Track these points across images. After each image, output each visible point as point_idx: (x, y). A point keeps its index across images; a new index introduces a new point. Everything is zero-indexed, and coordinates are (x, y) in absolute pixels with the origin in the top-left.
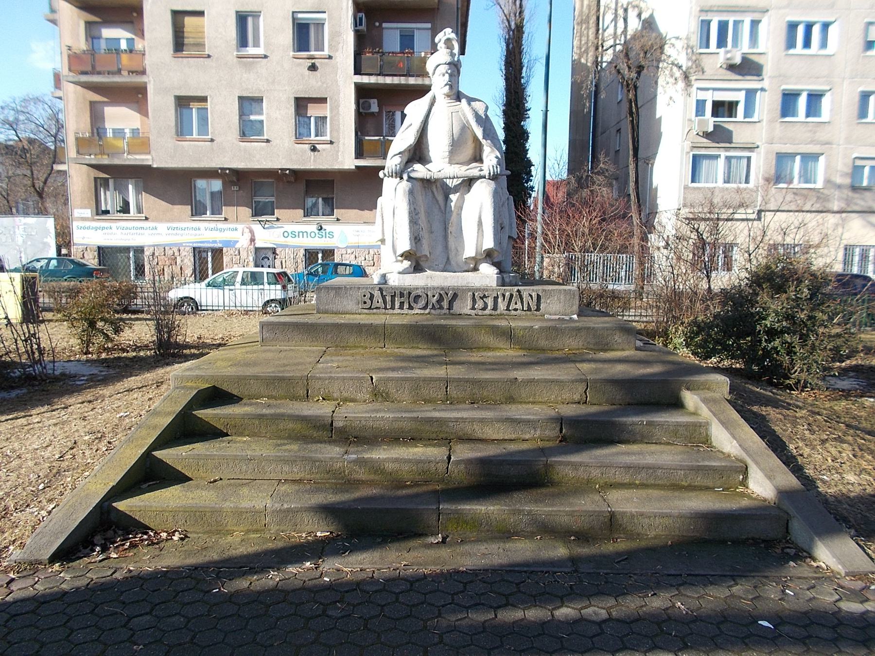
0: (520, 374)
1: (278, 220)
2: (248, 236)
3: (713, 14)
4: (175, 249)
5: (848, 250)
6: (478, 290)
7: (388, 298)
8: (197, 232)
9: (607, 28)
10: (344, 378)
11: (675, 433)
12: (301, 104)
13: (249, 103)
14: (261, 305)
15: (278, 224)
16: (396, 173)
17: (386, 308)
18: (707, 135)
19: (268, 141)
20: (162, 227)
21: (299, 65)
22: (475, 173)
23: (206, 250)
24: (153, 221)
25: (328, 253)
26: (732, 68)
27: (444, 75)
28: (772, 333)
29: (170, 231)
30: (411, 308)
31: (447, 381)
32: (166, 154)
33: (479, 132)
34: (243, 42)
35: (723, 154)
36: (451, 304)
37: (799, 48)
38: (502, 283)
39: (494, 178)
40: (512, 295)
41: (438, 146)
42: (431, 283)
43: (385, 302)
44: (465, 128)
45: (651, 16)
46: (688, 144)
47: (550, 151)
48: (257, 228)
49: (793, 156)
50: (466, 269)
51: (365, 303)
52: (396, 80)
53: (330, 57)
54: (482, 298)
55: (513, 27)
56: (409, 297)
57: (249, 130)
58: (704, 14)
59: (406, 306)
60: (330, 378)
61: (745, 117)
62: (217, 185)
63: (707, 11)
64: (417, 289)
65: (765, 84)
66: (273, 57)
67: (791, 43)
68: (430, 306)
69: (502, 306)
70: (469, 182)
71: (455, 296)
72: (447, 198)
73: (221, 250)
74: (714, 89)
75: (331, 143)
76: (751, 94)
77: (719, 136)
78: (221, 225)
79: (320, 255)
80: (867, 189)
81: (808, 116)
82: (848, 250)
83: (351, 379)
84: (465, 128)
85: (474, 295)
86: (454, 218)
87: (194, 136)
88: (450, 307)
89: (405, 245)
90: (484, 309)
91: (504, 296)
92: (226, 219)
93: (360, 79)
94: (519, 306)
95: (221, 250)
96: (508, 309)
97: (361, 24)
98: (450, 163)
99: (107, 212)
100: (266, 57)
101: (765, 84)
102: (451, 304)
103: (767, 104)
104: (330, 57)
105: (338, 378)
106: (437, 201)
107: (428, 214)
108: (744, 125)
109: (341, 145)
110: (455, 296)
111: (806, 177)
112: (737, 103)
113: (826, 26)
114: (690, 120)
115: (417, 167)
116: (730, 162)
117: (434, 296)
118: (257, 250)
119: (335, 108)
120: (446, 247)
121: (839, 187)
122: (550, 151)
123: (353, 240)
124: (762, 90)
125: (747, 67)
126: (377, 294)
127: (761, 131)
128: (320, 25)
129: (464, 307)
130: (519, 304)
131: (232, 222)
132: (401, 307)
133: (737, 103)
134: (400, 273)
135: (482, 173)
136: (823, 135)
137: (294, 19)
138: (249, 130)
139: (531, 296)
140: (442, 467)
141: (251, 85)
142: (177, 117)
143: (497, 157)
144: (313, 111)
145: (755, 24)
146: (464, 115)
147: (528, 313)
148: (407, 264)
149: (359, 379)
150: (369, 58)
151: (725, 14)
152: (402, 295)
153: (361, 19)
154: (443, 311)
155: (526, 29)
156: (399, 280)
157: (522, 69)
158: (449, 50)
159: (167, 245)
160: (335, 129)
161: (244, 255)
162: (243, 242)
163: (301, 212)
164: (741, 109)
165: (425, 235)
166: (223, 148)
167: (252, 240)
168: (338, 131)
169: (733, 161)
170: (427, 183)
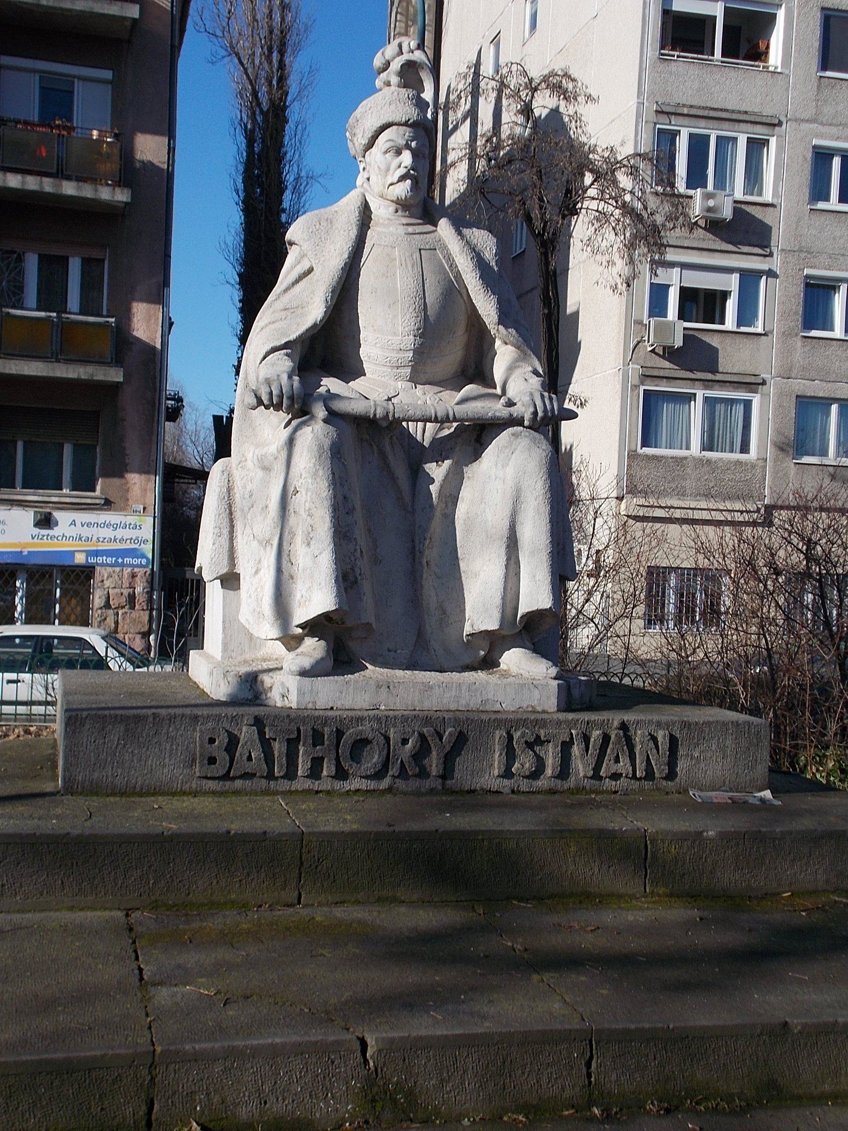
3: (680, 121)
6: (524, 723)
7: (278, 748)
9: (456, 128)
10: (275, 1052)
16: (291, 398)
17: (270, 776)
18: (670, 354)
26: (715, 226)
27: (399, 152)
30: (341, 774)
31: (590, 1040)
35: (700, 394)
36: (449, 760)
40: (606, 738)
41: (384, 334)
42: (387, 703)
43: (269, 757)
46: (634, 369)
49: (825, 403)
50: (467, 661)
51: (212, 761)
52: (32, 183)
54: (530, 745)
55: (265, 106)
58: (664, 119)
59: (327, 769)
60: (232, 1054)
61: (738, 326)
63: (668, 114)
64: (360, 720)
65: (776, 263)
67: (819, 191)
68: (394, 771)
69: (581, 767)
71: (461, 740)
74: (684, 266)
76: (750, 279)
77: (694, 357)
83: (299, 1050)
85: (510, 738)
86: (436, 526)
88: (447, 773)
89: (316, 597)
90: (536, 774)
91: (586, 739)
94: (624, 766)
96: (596, 776)
98: (415, 379)
101: (776, 263)
102: (449, 760)
103: (777, 301)
105: (256, 1052)
106: (393, 479)
108: (738, 339)
110: (461, 740)
112: (725, 295)
114: (639, 322)
115: (330, 384)
117: (405, 741)
120: (415, 601)
124: (771, 274)
125: (744, 229)
129: (487, 771)
130: (624, 762)
132: (315, 773)
134: (303, 673)
135: (516, 411)
139: (654, 739)
143: (535, 373)
146: (449, 258)
147: (647, 784)
149: (322, 1049)
151: (703, 123)
152: (317, 738)
154: (428, 784)
155: (294, 113)
156: (301, 693)
157: (282, 192)
158: (411, 92)
164: (731, 306)
165: (363, 565)
169: (720, 408)
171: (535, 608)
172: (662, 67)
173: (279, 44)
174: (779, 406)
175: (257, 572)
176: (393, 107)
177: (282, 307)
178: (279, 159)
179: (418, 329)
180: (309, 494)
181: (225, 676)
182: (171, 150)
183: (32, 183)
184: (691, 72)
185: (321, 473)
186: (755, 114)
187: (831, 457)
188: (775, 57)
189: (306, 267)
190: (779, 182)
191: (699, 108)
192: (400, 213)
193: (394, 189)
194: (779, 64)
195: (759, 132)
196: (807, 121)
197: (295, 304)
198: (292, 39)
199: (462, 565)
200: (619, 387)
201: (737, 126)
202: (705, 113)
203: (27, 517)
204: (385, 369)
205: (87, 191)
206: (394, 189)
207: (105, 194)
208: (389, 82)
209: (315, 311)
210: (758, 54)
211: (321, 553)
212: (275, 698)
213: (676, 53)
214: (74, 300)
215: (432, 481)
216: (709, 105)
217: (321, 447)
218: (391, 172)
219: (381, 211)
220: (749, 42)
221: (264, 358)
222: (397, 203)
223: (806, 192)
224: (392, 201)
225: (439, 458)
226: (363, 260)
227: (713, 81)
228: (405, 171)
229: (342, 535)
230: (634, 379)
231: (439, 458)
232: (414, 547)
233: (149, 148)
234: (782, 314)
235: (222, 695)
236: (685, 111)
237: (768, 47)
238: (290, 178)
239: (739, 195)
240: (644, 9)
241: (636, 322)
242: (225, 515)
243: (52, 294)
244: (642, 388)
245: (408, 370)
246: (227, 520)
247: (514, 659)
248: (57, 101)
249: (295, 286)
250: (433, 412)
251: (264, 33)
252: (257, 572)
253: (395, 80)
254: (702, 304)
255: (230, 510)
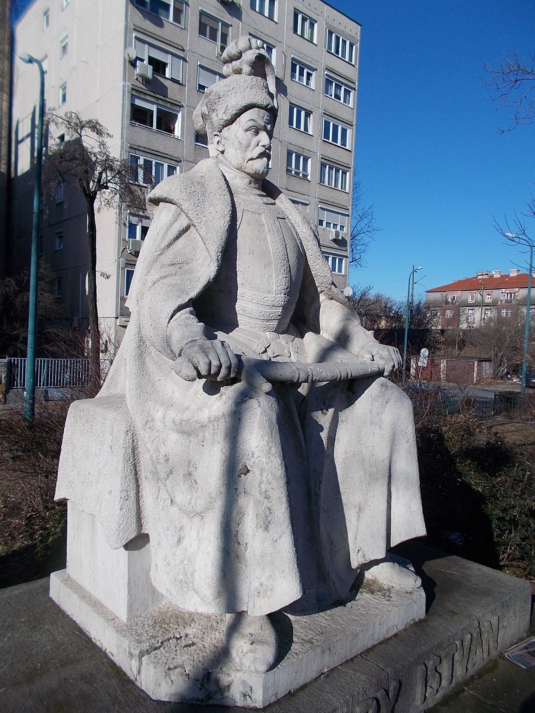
3: (140, 153)
58: (133, 151)
171: (414, 536)
172: (131, 128)
175: (179, 541)
176: (254, 90)
177: (168, 262)
179: (287, 288)
180: (265, 475)
181: (167, 674)
184: (144, 133)
185: (274, 450)
186: (171, 155)
188: (178, 132)
189: (185, 225)
191: (148, 149)
192: (252, 185)
193: (252, 165)
194: (179, 136)
195: (173, 163)
196: (191, 162)
197: (180, 260)
199: (344, 498)
200: (116, 268)
201: (164, 159)
202: (151, 151)
204: (257, 321)
206: (252, 165)
208: (241, 70)
210: (171, 131)
211: (280, 537)
213: (137, 124)
215: (322, 429)
216: (151, 148)
217: (271, 423)
218: (251, 148)
220: (166, 124)
221: (172, 317)
222: (252, 177)
224: (248, 174)
225: (323, 407)
226: (238, 223)
228: (263, 149)
231: (324, 407)
232: (309, 490)
235: (163, 694)
236: (142, 149)
237: (174, 128)
240: (123, 101)
241: (123, 240)
242: (131, 477)
244: (126, 269)
245: (276, 323)
246: (133, 481)
249: (176, 242)
250: (338, 372)
252: (179, 541)
253: (246, 69)
255: (135, 470)
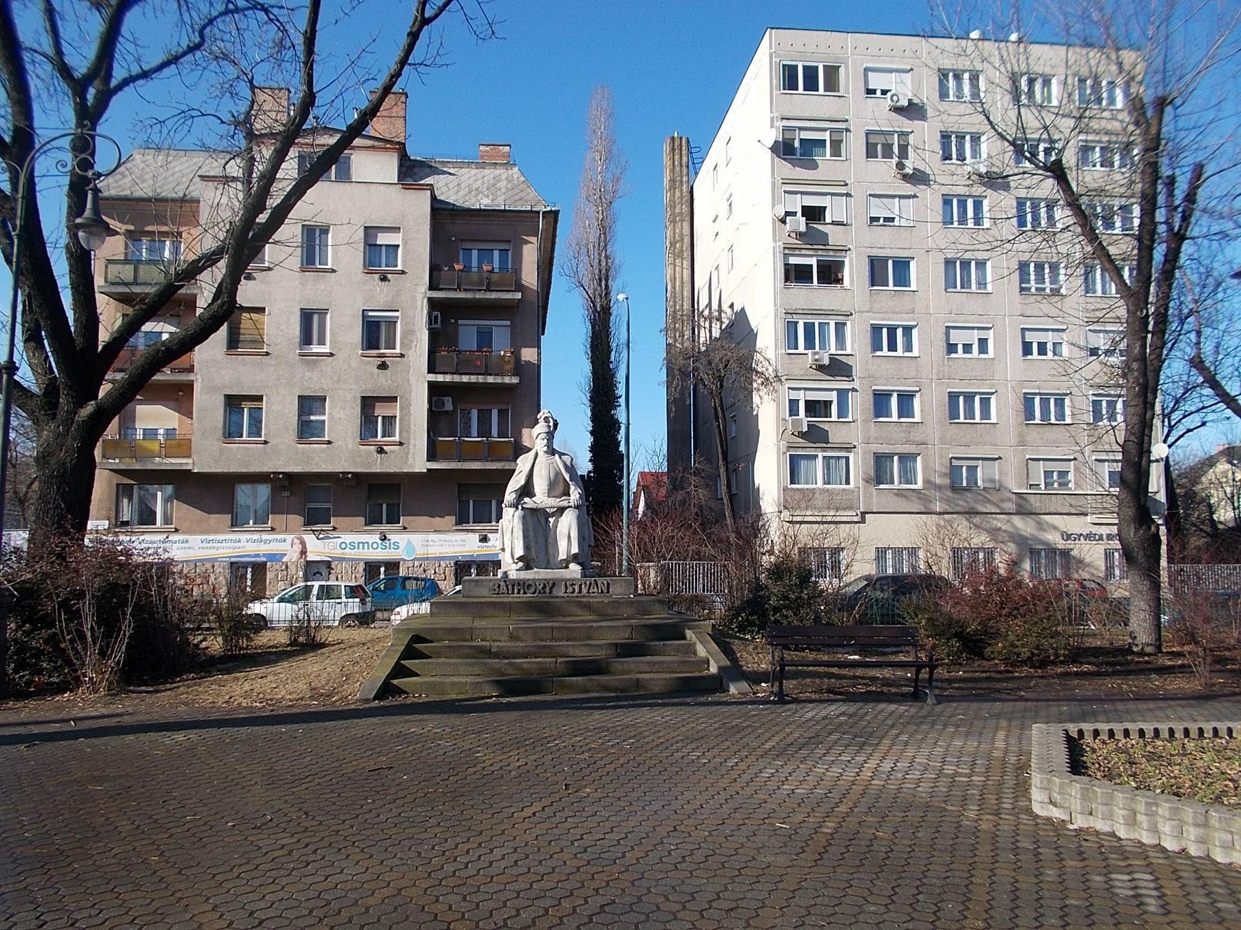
0: (594, 625)
1: (335, 529)
2: (298, 548)
4: (208, 565)
5: (881, 553)
8: (237, 545)
11: (678, 650)
12: (368, 403)
13: (309, 404)
14: (338, 618)
15: (335, 534)
18: (802, 435)
19: (329, 442)
20: (195, 540)
21: (369, 363)
22: (565, 504)
23: (245, 566)
24: (184, 533)
25: (393, 566)
26: (821, 368)
28: (776, 610)
29: (205, 545)
31: (553, 628)
32: (210, 455)
33: (567, 477)
34: (306, 339)
35: (820, 455)
37: (885, 352)
38: (584, 575)
39: (577, 507)
41: (540, 486)
44: (558, 474)
45: (743, 309)
46: (783, 444)
47: (647, 443)
48: (310, 539)
49: (890, 456)
52: (473, 379)
53: (402, 356)
56: (523, 585)
57: (307, 430)
62: (264, 491)
65: (856, 384)
66: (340, 356)
67: (877, 346)
69: (584, 590)
70: (561, 510)
71: (554, 584)
72: (547, 521)
73: (264, 565)
75: (401, 444)
76: (842, 394)
77: (815, 435)
78: (265, 536)
79: (382, 569)
80: (965, 489)
81: (899, 417)
82: (881, 553)
84: (558, 474)
87: (244, 438)
89: (520, 552)
92: (273, 529)
93: (432, 377)
95: (264, 565)
97: (436, 323)
99: (126, 524)
100: (331, 355)
103: (859, 404)
104: (402, 356)
107: (535, 530)
109: (411, 447)
110: (554, 584)
111: (908, 476)
112: (831, 402)
113: (908, 330)
115: (526, 499)
116: (829, 464)
118: (309, 563)
119: (406, 408)
120: (547, 553)
121: (939, 488)
122: (647, 443)
123: (420, 551)
124: (854, 390)
125: (837, 368)
126: (502, 583)
127: (855, 429)
128: (392, 323)
129: (560, 592)
131: (280, 533)
133: (831, 402)
136: (917, 435)
137: (364, 316)
138: (307, 430)
140: (553, 666)
141: (313, 382)
142: (225, 417)
144: (381, 411)
145: (840, 327)
148: (521, 564)
150: (444, 356)
153: (436, 317)
159: (200, 560)
160: (405, 430)
161: (292, 569)
162: (292, 555)
163: (361, 520)
164: (834, 408)
165: (533, 544)
166: (281, 451)
167: (303, 552)
168: (408, 432)
170: (534, 511)
173: (604, 277)
174: (864, 459)
178: (608, 335)
182: (539, 354)
183: (473, 379)
187: (896, 485)
190: (855, 345)
198: (611, 273)
203: (476, 537)
205: (499, 380)
207: (507, 380)
209: (523, 482)
212: (511, 577)
214: (495, 431)
219: (541, 454)
223: (869, 348)
227: (815, 295)
229: (525, 537)
230: (783, 449)
233: (528, 354)
234: (862, 411)
238: (614, 345)
239: (833, 351)
243: (484, 431)
247: (573, 566)
248: (485, 338)
251: (597, 272)
254: (815, 408)
